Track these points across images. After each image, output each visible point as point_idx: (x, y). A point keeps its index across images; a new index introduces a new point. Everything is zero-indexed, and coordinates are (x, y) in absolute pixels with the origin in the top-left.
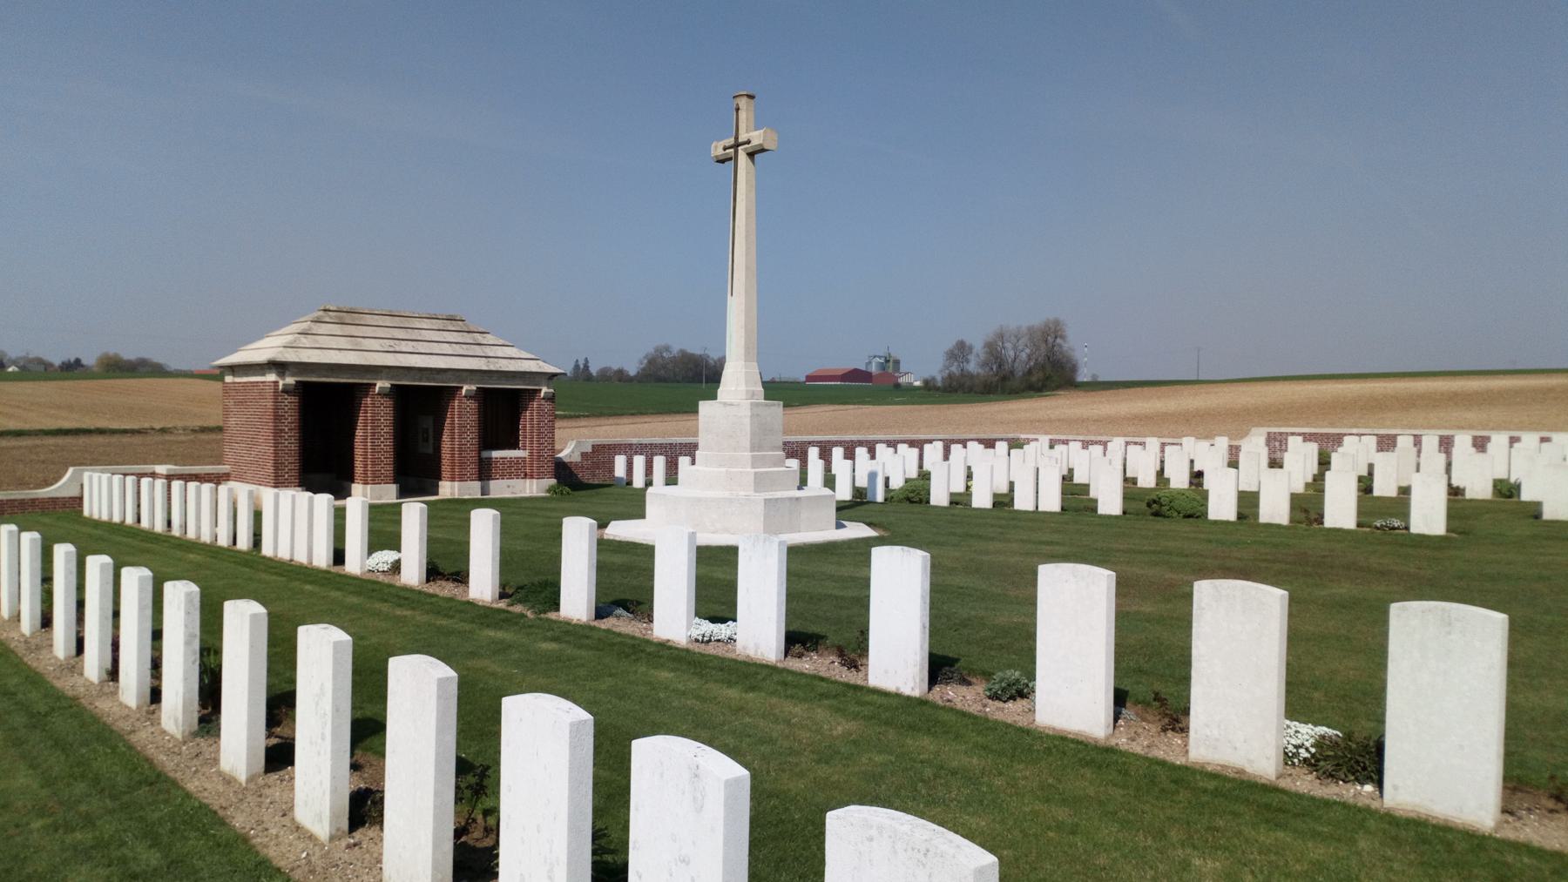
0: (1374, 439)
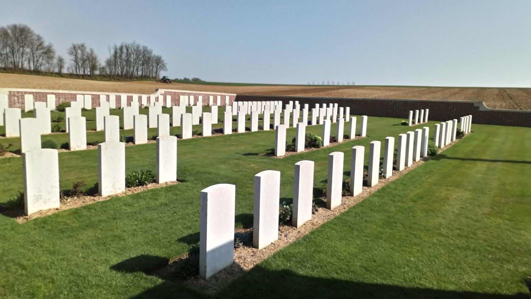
0: (90, 96)
